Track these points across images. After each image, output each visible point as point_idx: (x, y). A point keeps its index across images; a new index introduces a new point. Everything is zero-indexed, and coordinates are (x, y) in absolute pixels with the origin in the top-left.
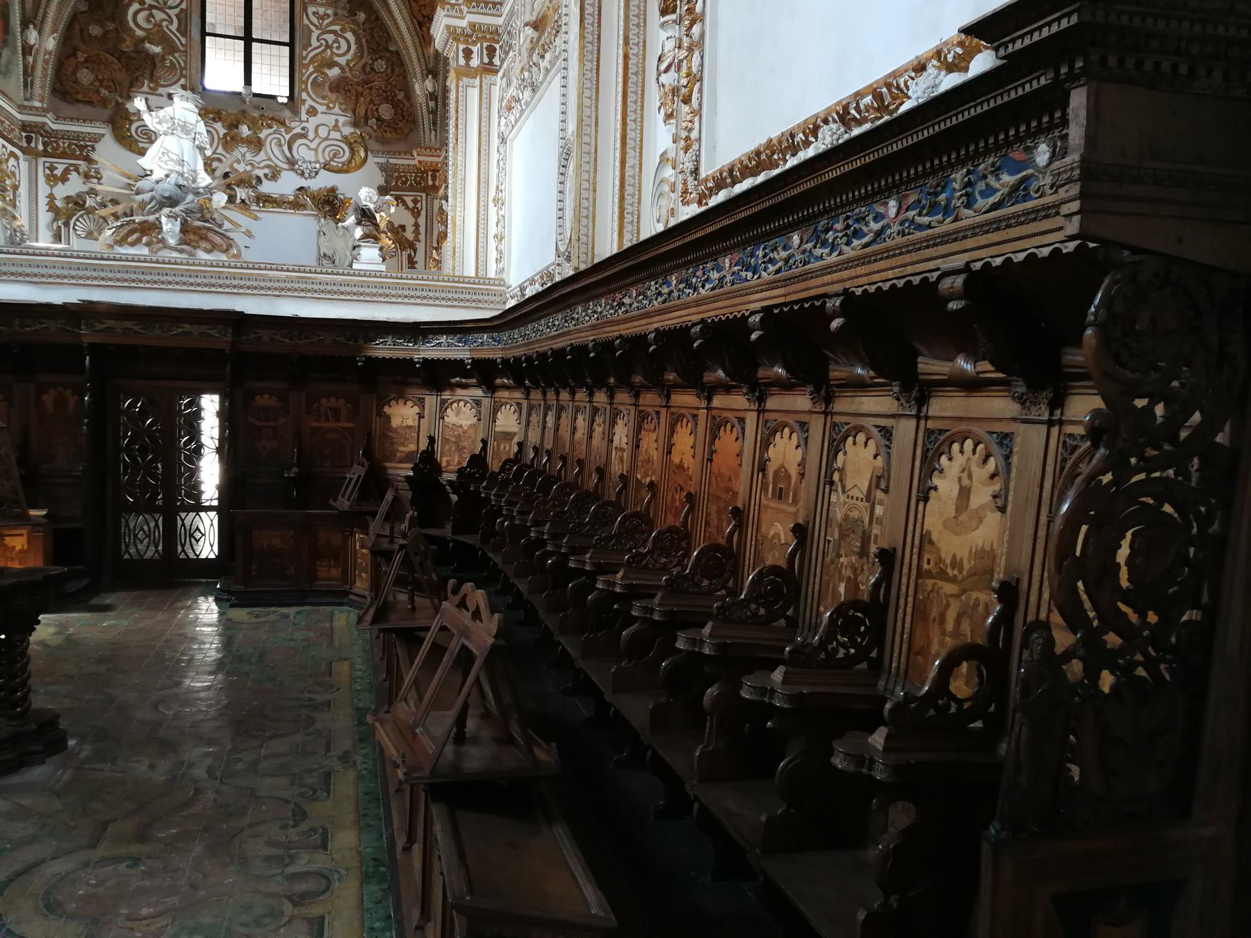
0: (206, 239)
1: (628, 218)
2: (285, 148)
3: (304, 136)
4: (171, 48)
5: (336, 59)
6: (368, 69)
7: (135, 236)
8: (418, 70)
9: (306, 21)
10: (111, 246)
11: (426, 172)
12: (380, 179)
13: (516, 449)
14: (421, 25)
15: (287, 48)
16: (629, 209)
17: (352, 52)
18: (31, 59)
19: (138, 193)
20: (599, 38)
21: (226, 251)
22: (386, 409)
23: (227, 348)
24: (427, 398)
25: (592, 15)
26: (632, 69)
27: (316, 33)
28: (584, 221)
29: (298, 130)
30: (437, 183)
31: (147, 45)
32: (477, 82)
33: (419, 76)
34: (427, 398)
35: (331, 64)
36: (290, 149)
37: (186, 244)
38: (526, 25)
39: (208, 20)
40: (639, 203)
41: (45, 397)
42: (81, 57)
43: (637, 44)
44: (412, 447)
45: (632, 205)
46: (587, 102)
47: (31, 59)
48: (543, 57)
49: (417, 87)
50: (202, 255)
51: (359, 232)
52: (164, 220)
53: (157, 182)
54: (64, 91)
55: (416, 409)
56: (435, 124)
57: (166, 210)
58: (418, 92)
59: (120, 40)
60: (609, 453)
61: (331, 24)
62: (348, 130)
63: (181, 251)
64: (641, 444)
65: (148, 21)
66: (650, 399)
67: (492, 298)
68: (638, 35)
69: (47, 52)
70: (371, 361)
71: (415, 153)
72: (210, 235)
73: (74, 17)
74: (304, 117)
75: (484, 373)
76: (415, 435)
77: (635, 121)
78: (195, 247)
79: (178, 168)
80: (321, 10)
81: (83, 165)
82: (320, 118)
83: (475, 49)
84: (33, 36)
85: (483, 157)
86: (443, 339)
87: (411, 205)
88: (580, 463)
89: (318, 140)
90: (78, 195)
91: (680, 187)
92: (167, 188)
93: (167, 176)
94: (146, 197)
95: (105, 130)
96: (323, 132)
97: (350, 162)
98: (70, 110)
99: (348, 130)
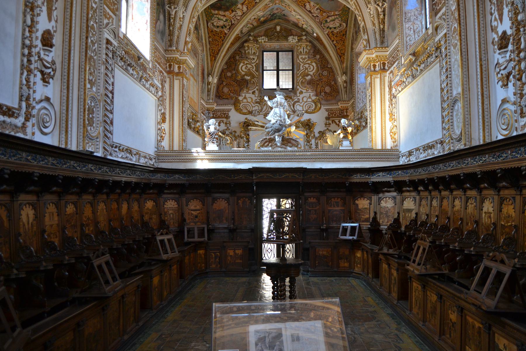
0: (290, 142)
1: (486, 124)
2: (292, 107)
3: (298, 102)
4: (253, 77)
5: (309, 73)
6: (321, 75)
7: (267, 144)
8: (339, 73)
9: (298, 61)
10: (259, 148)
11: (343, 110)
12: (326, 114)
13: (414, 215)
14: (340, 57)
15: (291, 72)
16: (486, 120)
17: (315, 69)
18: (210, 86)
19: (266, 129)
20: (468, 60)
21: (297, 146)
22: (356, 202)
23: (301, 181)
24: (373, 197)
25: (465, 52)
26: (484, 69)
27: (302, 64)
28: (467, 126)
29: (296, 100)
30: (348, 114)
31: (246, 77)
32: (379, 76)
33: (340, 75)
34: (373, 197)
35: (308, 75)
36: (294, 107)
37: (283, 145)
38: (410, 55)
39: (265, 65)
40: (490, 118)
41: (239, 201)
42: (224, 83)
43: (485, 60)
44: (367, 216)
45: (487, 119)
46: (465, 83)
47: (210, 86)
48: (419, 66)
49: (339, 79)
50: (289, 149)
51: (342, 136)
52: (276, 137)
53: (273, 124)
54: (219, 96)
55: (368, 201)
56: (346, 92)
57: (277, 134)
58: (340, 81)
59: (237, 76)
60: (480, 215)
61: (307, 61)
62: (314, 98)
63: (281, 148)
64: (503, 210)
65: (246, 69)
66: (445, 193)
67: (393, 157)
68: (485, 57)
69: (214, 84)
70: (351, 183)
71: (339, 103)
72: (292, 141)
73: (222, 71)
74: (298, 95)
75: (399, 187)
76: (368, 211)
77: (486, 88)
78: (286, 146)
79: (280, 119)
80: (304, 57)
81: (225, 120)
82: (304, 95)
83: (377, 64)
84: (210, 79)
85: (383, 103)
86: (381, 174)
87: (338, 123)
88: (461, 219)
89: (303, 103)
90: (223, 130)
91: (519, 112)
92: (277, 126)
93: (276, 122)
94: (270, 129)
95: (232, 107)
96: (305, 99)
97: (315, 109)
98: (221, 102)
99: (314, 98)
